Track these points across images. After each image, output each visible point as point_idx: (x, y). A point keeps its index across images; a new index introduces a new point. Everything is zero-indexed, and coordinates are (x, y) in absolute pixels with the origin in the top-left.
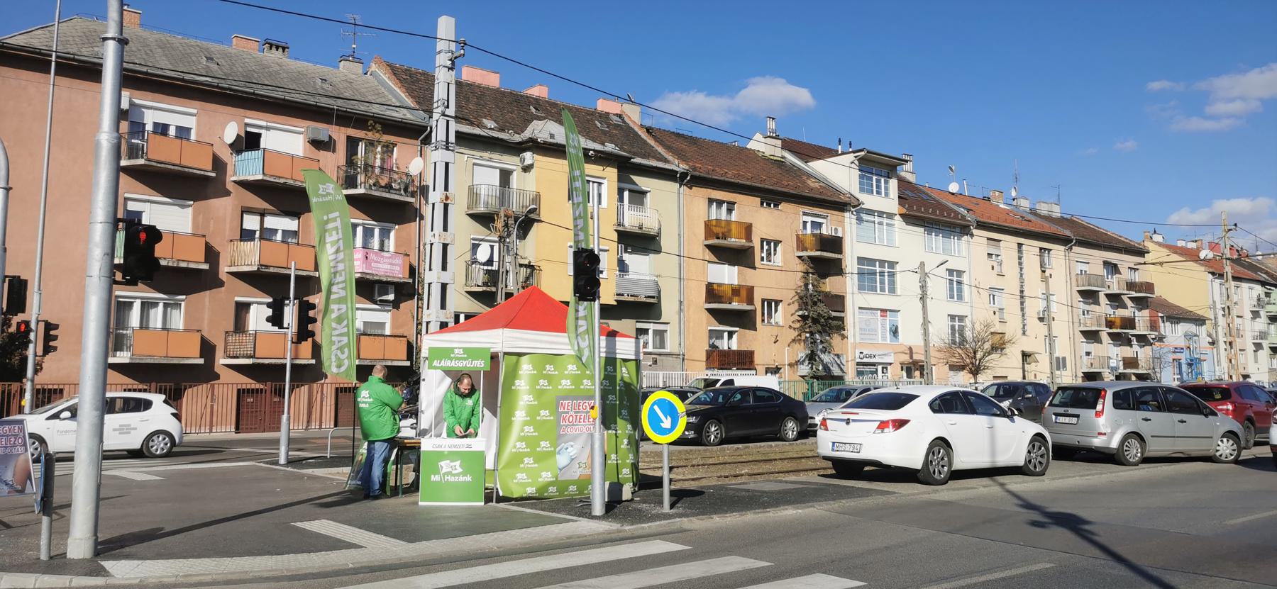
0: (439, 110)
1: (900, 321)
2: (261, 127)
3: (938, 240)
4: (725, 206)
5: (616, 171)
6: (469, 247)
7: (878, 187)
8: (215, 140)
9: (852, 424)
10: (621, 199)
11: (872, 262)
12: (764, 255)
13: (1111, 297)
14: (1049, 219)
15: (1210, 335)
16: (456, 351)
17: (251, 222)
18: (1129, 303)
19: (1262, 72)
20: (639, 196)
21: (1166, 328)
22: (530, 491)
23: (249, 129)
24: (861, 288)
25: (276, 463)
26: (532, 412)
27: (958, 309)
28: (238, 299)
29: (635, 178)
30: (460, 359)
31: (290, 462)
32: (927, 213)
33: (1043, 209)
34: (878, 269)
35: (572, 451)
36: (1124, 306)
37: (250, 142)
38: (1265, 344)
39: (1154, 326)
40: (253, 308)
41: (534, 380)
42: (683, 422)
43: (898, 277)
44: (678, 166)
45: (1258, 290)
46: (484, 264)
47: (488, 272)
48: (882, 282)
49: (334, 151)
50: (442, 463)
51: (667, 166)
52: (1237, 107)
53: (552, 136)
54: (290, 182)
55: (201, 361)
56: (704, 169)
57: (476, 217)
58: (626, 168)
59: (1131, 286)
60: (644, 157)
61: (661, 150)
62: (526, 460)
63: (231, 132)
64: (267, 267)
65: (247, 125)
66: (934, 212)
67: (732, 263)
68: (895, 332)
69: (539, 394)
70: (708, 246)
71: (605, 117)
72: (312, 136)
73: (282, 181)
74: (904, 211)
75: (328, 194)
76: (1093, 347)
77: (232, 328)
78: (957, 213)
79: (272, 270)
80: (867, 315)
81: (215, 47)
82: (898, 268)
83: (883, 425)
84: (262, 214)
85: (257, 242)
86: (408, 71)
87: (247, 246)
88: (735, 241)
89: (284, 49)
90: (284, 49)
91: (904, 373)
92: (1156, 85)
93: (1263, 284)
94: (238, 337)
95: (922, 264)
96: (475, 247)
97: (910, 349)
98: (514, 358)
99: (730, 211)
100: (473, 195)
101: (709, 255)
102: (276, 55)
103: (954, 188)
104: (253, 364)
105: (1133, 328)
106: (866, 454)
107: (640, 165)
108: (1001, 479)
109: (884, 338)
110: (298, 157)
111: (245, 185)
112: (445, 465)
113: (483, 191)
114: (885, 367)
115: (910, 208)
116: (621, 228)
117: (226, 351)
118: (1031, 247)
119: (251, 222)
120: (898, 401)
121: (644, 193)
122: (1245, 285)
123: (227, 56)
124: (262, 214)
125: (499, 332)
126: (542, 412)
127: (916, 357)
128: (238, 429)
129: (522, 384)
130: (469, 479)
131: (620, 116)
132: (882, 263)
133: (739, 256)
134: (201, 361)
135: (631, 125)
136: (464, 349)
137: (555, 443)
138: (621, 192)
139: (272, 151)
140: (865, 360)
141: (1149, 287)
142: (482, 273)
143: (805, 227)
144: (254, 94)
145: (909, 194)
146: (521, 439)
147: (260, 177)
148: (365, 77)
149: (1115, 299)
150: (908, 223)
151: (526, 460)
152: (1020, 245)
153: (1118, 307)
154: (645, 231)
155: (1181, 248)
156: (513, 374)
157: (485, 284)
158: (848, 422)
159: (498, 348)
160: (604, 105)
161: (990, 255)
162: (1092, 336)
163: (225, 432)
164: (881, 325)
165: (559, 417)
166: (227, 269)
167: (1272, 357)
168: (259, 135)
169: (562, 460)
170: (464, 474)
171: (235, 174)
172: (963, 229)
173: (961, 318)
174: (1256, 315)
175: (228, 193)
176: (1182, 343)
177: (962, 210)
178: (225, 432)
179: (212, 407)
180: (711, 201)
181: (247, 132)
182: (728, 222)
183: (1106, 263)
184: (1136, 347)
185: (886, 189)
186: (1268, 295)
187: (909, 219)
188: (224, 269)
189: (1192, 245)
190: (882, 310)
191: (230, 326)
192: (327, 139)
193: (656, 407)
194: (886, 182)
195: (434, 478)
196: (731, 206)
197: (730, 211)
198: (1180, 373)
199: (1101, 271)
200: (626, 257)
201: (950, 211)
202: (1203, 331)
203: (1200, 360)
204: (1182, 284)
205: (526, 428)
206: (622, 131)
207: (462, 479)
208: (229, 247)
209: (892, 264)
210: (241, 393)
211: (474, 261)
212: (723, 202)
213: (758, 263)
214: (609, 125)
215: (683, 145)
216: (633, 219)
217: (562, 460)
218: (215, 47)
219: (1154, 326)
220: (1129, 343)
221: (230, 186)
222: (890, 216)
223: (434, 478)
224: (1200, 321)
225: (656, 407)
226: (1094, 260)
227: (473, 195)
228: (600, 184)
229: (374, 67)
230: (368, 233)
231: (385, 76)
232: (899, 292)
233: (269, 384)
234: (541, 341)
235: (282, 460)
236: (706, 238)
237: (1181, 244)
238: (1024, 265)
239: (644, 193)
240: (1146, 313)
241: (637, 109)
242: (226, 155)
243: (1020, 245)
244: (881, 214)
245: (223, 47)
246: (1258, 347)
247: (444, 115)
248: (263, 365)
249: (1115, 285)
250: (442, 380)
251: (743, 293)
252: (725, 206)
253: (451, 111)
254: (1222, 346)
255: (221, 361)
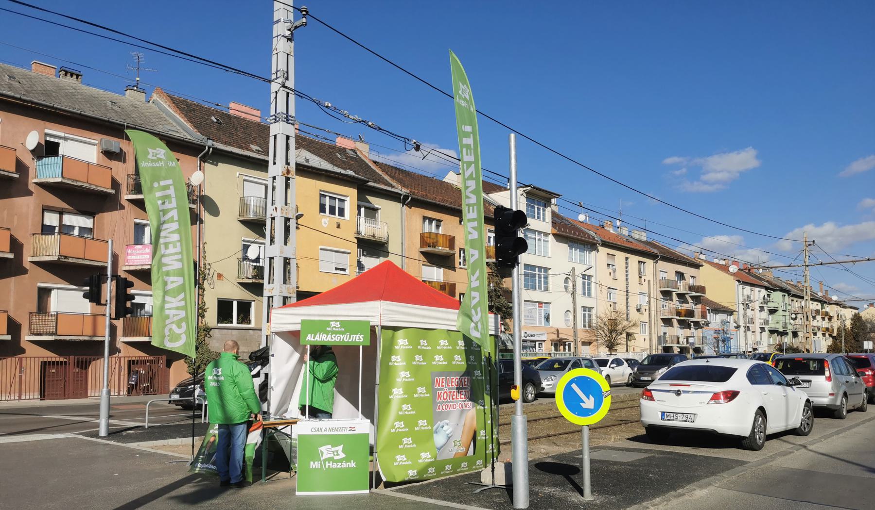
0: (280, 80)
1: (552, 310)
2: (60, 137)
3: (576, 253)
4: (434, 223)
5: (355, 191)
6: (241, 248)
7: (539, 214)
8: (19, 147)
9: (683, 395)
10: (359, 214)
11: (533, 267)
12: (461, 260)
13: (679, 295)
14: (640, 241)
15: (735, 322)
16: (333, 324)
17: (51, 219)
18: (690, 300)
19: (738, 154)
20: (372, 212)
21: (710, 317)
22: (412, 473)
23: (48, 139)
24: (526, 286)
25: (96, 435)
26: (409, 388)
27: (588, 302)
28: (40, 284)
29: (370, 198)
30: (336, 333)
31: (114, 433)
32: (569, 234)
33: (636, 235)
34: (537, 273)
35: (448, 429)
36: (687, 302)
37: (49, 149)
38: (767, 328)
39: (704, 316)
40: (54, 293)
41: (410, 356)
42: (607, 403)
43: (550, 279)
44: (403, 191)
45: (764, 292)
46: (253, 261)
47: (255, 267)
48: (540, 282)
49: (124, 162)
50: (323, 449)
51: (393, 190)
52: (719, 176)
53: (307, 161)
54: (86, 185)
55: (9, 338)
56: (420, 195)
57: (247, 223)
58: (364, 190)
59: (691, 288)
60: (375, 182)
61: (386, 177)
62: (405, 440)
63: (33, 140)
64: (66, 257)
65: (47, 135)
66: (575, 233)
67: (439, 266)
68: (547, 318)
69: (416, 370)
70: (422, 253)
71: (343, 151)
72: (105, 147)
73: (79, 184)
74: (556, 231)
75: (159, 160)
76: (668, 330)
77: (35, 310)
78: (589, 235)
79: (70, 260)
80: (530, 306)
81: (17, 70)
82: (550, 272)
83: (716, 397)
84: (61, 213)
85: (57, 236)
86: (184, 102)
87: (48, 239)
88: (442, 249)
89: (78, 76)
90: (78, 76)
91: (553, 348)
92: (669, 161)
93: (767, 288)
94: (41, 317)
95: (574, 269)
96: (246, 248)
97: (558, 330)
98: (390, 332)
99: (438, 226)
100: (244, 205)
101: (422, 258)
102: (70, 81)
103: (582, 218)
104: (56, 341)
105: (693, 316)
106: (701, 423)
107: (374, 187)
108: (784, 438)
109: (540, 322)
110: (92, 164)
111: (45, 186)
112: (326, 451)
113: (252, 202)
114: (541, 342)
115: (560, 230)
116: (359, 236)
117: (30, 329)
118: (634, 259)
119: (51, 219)
120: (725, 374)
121: (375, 210)
122: (756, 289)
123: (25, 77)
124: (61, 213)
125: (377, 303)
126: (419, 389)
127: (561, 336)
128: (43, 396)
129: (398, 360)
130: (353, 464)
131: (354, 151)
132: (540, 268)
133: (444, 261)
134: (9, 338)
135: (363, 158)
136: (341, 322)
137: (431, 423)
138: (359, 207)
139: (69, 158)
140: (528, 338)
141: (702, 289)
142: (251, 268)
143: (489, 241)
144: (53, 107)
145: (557, 221)
146: (399, 418)
147: (59, 180)
148: (148, 105)
149: (681, 296)
150: (557, 241)
151: (405, 440)
152: (627, 259)
153: (683, 303)
154: (377, 239)
155: (717, 264)
156: (389, 350)
157: (254, 277)
158: (678, 393)
159: (375, 321)
160: (341, 142)
161: (608, 265)
162: (667, 322)
163: (31, 399)
164: (538, 313)
165: (434, 393)
166: (30, 259)
167: (770, 336)
168: (58, 145)
169: (439, 439)
170: (347, 459)
171: (36, 177)
172: (590, 245)
173: (590, 309)
174: (762, 309)
175: (30, 193)
176: (719, 327)
177: (591, 233)
178: (31, 399)
179: (21, 377)
180: (425, 218)
181: (47, 142)
182: (437, 234)
183: (677, 273)
184: (693, 330)
185: (544, 215)
186: (769, 296)
187: (559, 237)
188: (28, 259)
189: (722, 262)
190: (540, 303)
191: (34, 309)
192: (118, 151)
193: (574, 386)
194: (544, 210)
195: (314, 465)
196: (439, 222)
197: (438, 226)
198: (718, 347)
199: (674, 278)
200: (363, 260)
201: (585, 233)
202: (731, 319)
203: (729, 339)
204: (720, 287)
205: (405, 407)
206: (357, 162)
207: (344, 465)
208: (32, 239)
209: (547, 269)
210: (45, 365)
211: (245, 258)
212: (434, 219)
213: (457, 265)
214: (347, 157)
215: (401, 176)
216: (367, 229)
217: (439, 439)
218: (17, 70)
219: (704, 316)
220: (689, 327)
221: (32, 187)
222: (546, 234)
223: (314, 465)
224: (730, 312)
225: (574, 386)
226: (669, 270)
227: (244, 205)
228: (343, 201)
229: (155, 97)
230: (539, 209)
231: (166, 104)
232: (550, 289)
233: (72, 357)
234: (430, 317)
235: (103, 432)
236: (421, 247)
237: (716, 261)
238: (629, 273)
239: (375, 210)
240: (699, 306)
241: (367, 147)
242: (28, 160)
243: (627, 259)
244: (540, 233)
245: (24, 71)
246: (763, 330)
247: (284, 86)
248: (64, 341)
249: (682, 288)
250: (291, 355)
251: (447, 288)
252: (434, 223)
253: (290, 83)
254: (742, 329)
255: (26, 337)
